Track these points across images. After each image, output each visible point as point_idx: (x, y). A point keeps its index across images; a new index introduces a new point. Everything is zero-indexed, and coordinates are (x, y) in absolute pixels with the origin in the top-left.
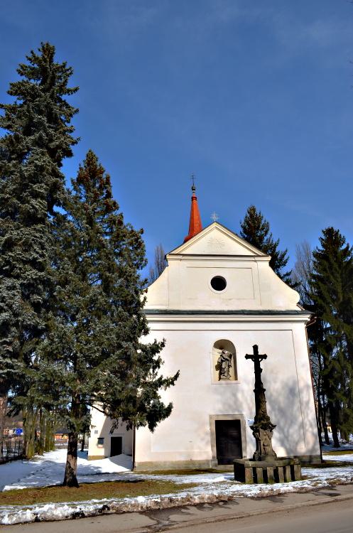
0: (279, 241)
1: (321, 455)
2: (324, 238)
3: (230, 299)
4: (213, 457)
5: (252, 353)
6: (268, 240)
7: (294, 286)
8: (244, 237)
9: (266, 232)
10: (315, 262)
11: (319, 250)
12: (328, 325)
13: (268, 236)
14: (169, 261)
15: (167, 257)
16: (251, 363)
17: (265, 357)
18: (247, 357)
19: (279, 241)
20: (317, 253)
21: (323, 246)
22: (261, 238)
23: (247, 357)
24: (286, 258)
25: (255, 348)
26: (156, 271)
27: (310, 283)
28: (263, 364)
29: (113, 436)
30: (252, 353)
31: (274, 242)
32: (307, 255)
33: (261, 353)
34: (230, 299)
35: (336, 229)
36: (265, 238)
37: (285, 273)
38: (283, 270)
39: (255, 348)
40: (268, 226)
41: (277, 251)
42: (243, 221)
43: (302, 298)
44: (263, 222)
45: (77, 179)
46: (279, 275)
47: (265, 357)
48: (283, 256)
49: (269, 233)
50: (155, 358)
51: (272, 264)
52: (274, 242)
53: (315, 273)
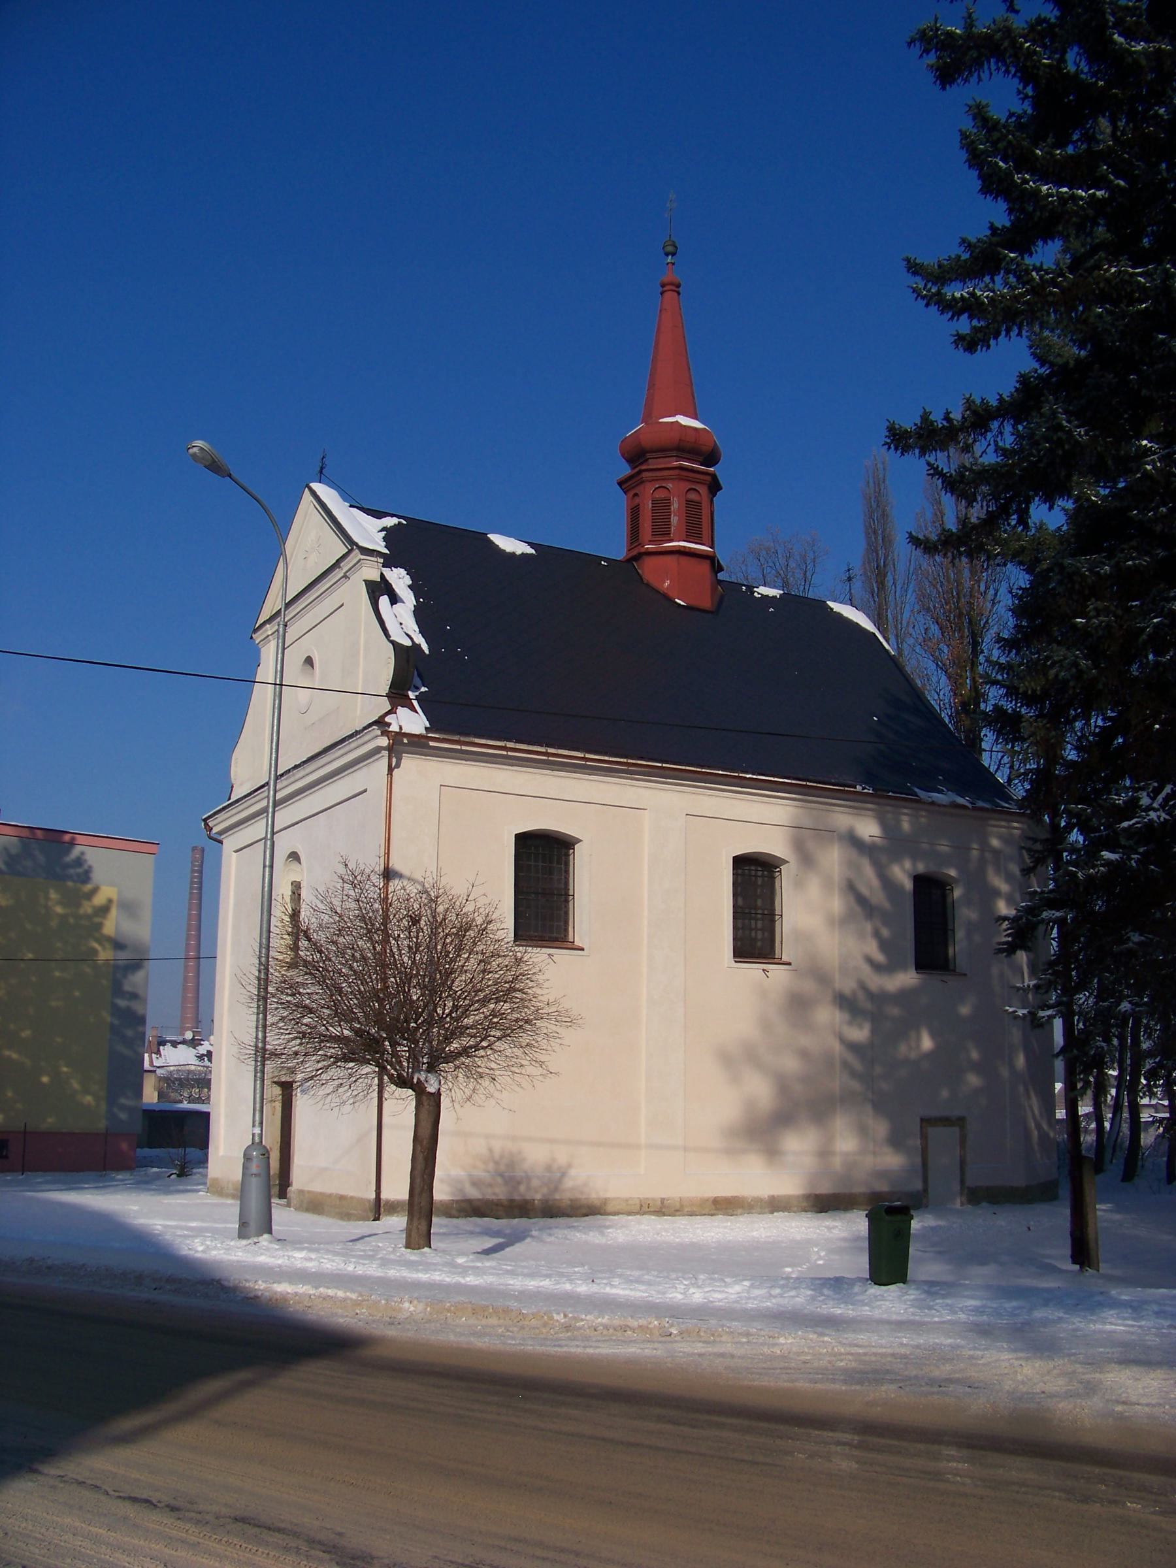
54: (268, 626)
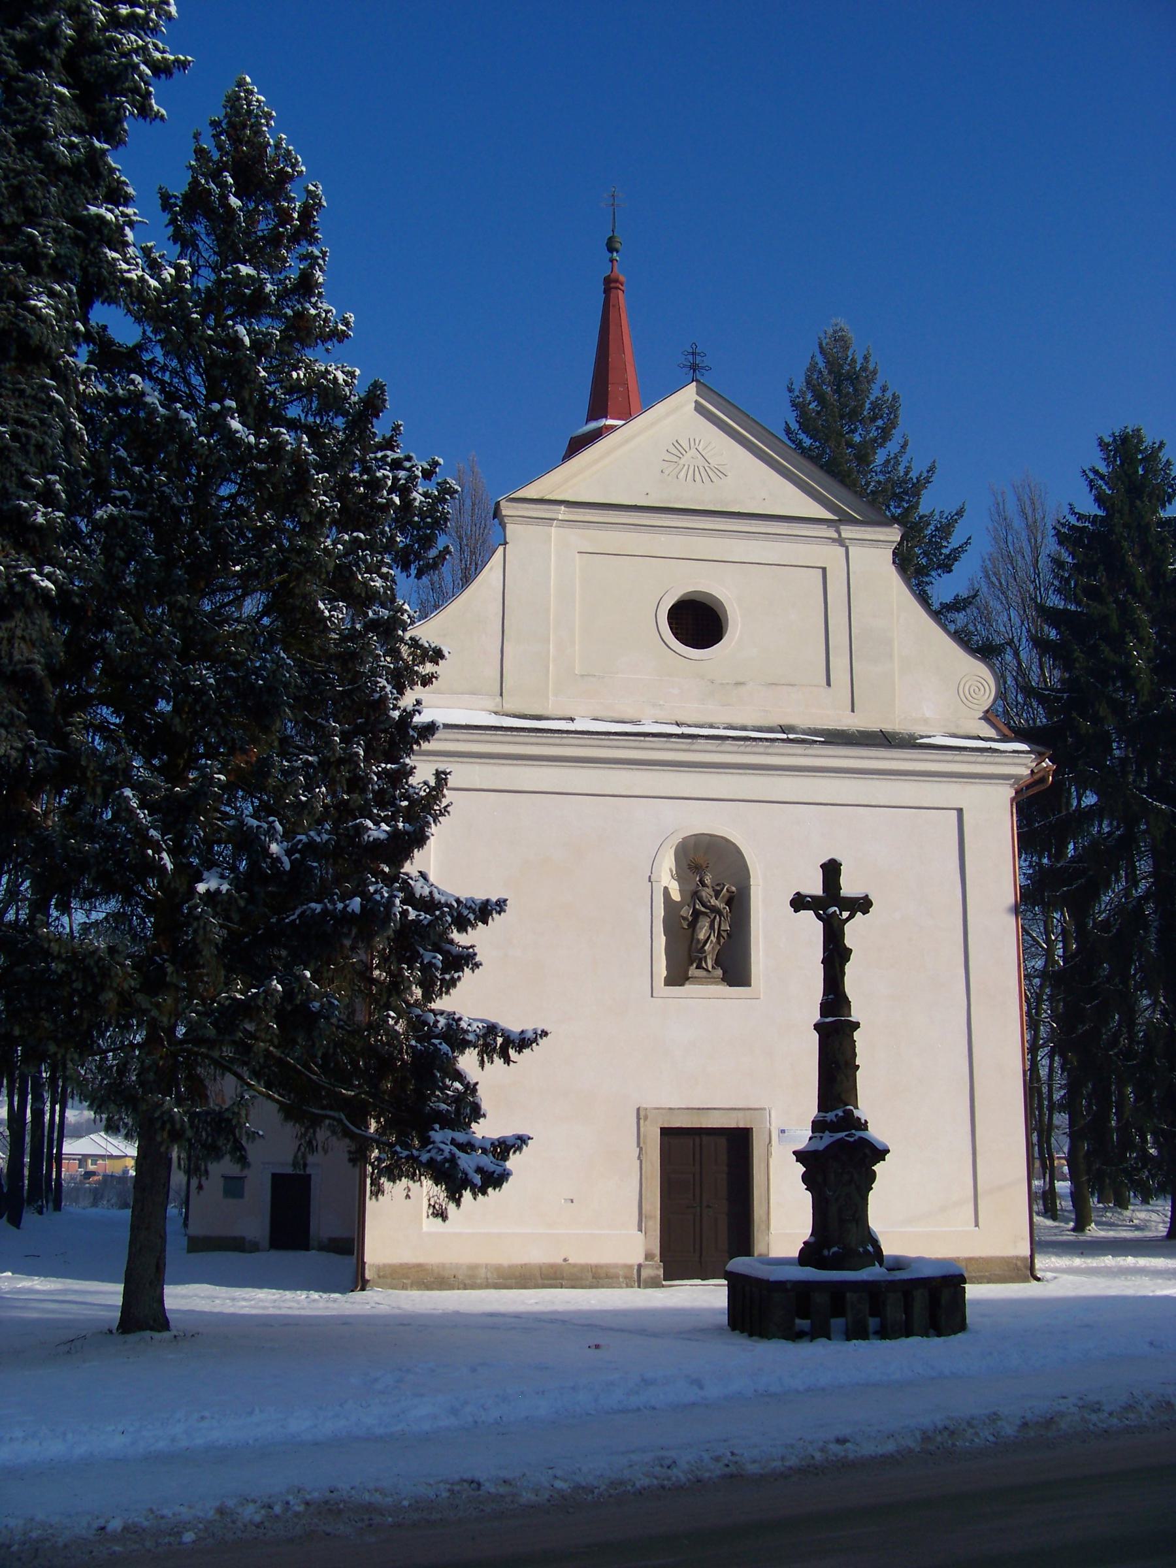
0: (931, 469)
1: (1032, 1257)
2: (1103, 469)
3: (739, 684)
4: (648, 1256)
5: (815, 888)
6: (891, 463)
7: (985, 651)
8: (799, 445)
9: (885, 435)
10: (1058, 563)
11: (1080, 517)
12: (1090, 799)
13: (892, 447)
14: (509, 527)
15: (504, 512)
16: (810, 926)
17: (862, 905)
18: (799, 903)
19: (931, 469)
20: (1072, 528)
21: (1100, 500)
22: (863, 456)
23: (799, 903)
24: (955, 541)
25: (831, 870)
26: (981, 634)
27: (1040, 644)
28: (855, 931)
29: (266, 1242)
30: (815, 888)
31: (913, 475)
32: (1032, 529)
33: (849, 887)
34: (739, 684)
35: (1149, 438)
36: (880, 457)
37: (948, 599)
38: (944, 588)
39: (831, 870)
40: (893, 410)
41: (923, 509)
42: (800, 383)
43: (1001, 695)
44: (875, 393)
45: (186, 198)
46: (923, 599)
47: (862, 905)
48: (945, 530)
49: (897, 435)
50: (460, 938)
51: (903, 560)
52: (913, 475)
53: (1055, 601)
54: (563, 508)
